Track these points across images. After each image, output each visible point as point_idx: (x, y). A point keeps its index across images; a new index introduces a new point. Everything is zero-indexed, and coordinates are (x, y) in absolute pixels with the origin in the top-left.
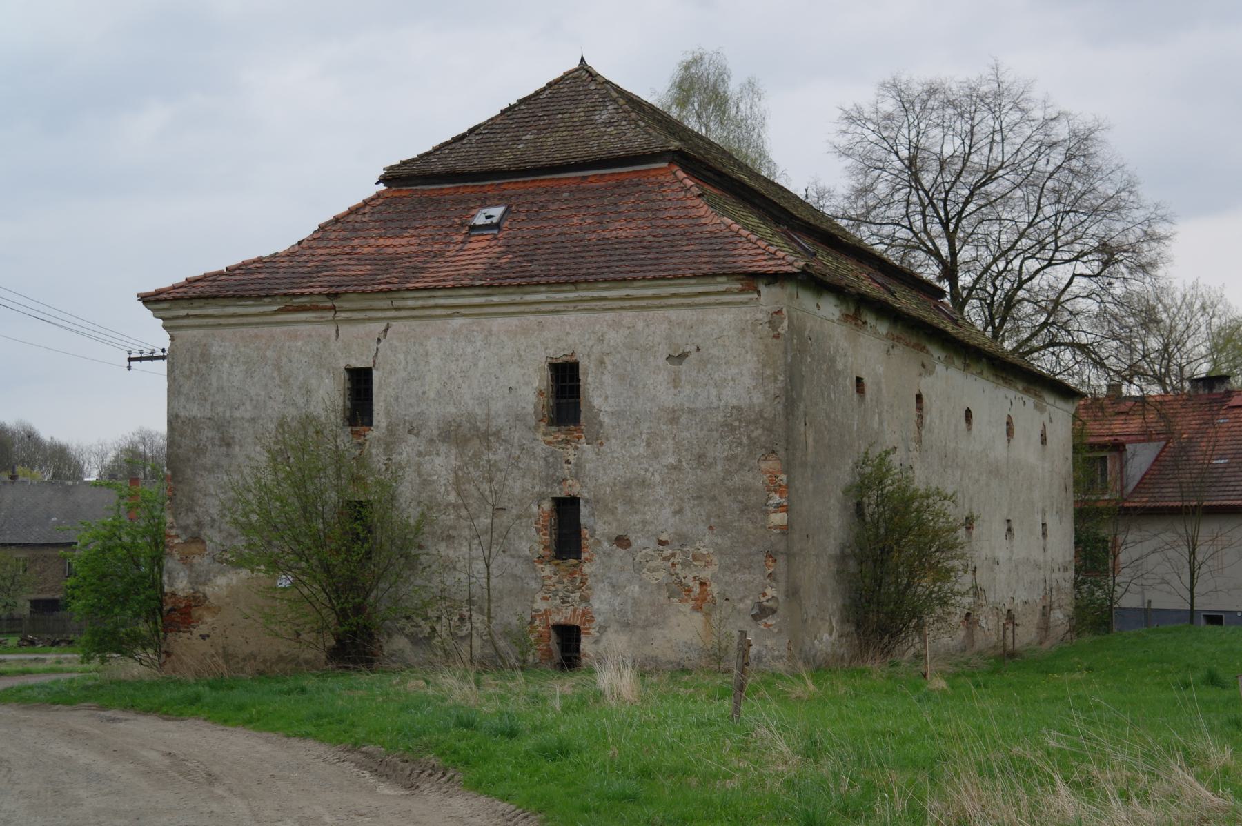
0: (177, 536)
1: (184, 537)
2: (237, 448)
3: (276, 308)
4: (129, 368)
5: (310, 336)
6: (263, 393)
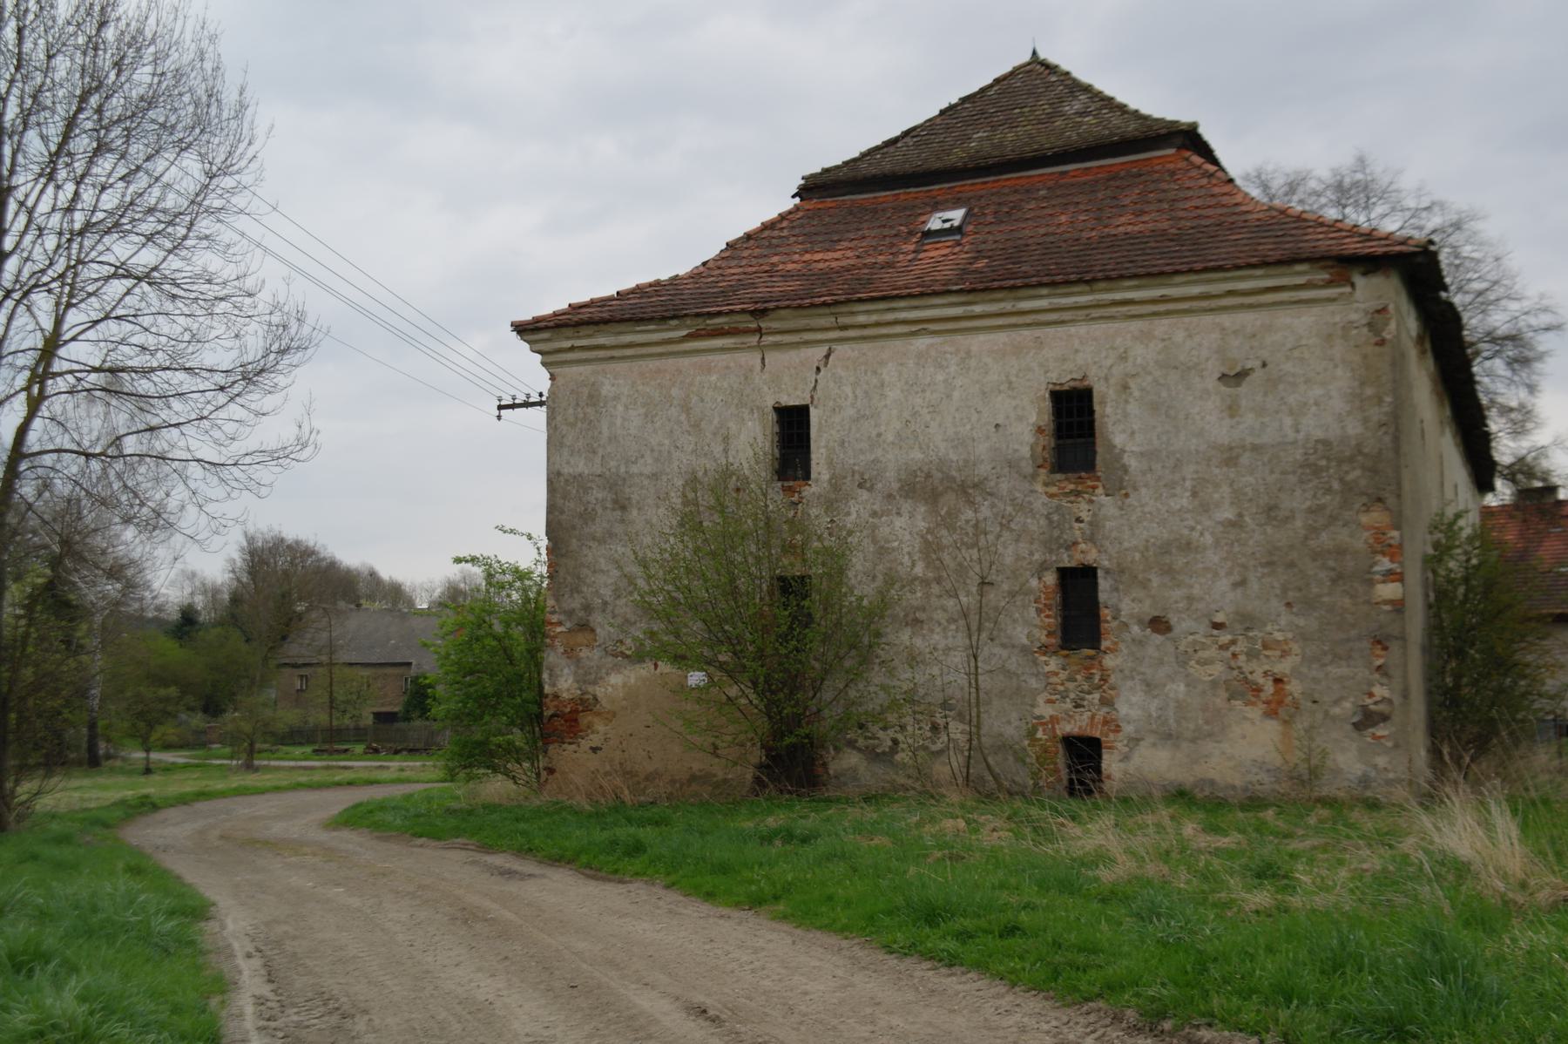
0: (560, 623)
1: (568, 625)
2: (635, 512)
3: (685, 333)
4: (499, 417)
5: (728, 367)
6: (667, 442)
